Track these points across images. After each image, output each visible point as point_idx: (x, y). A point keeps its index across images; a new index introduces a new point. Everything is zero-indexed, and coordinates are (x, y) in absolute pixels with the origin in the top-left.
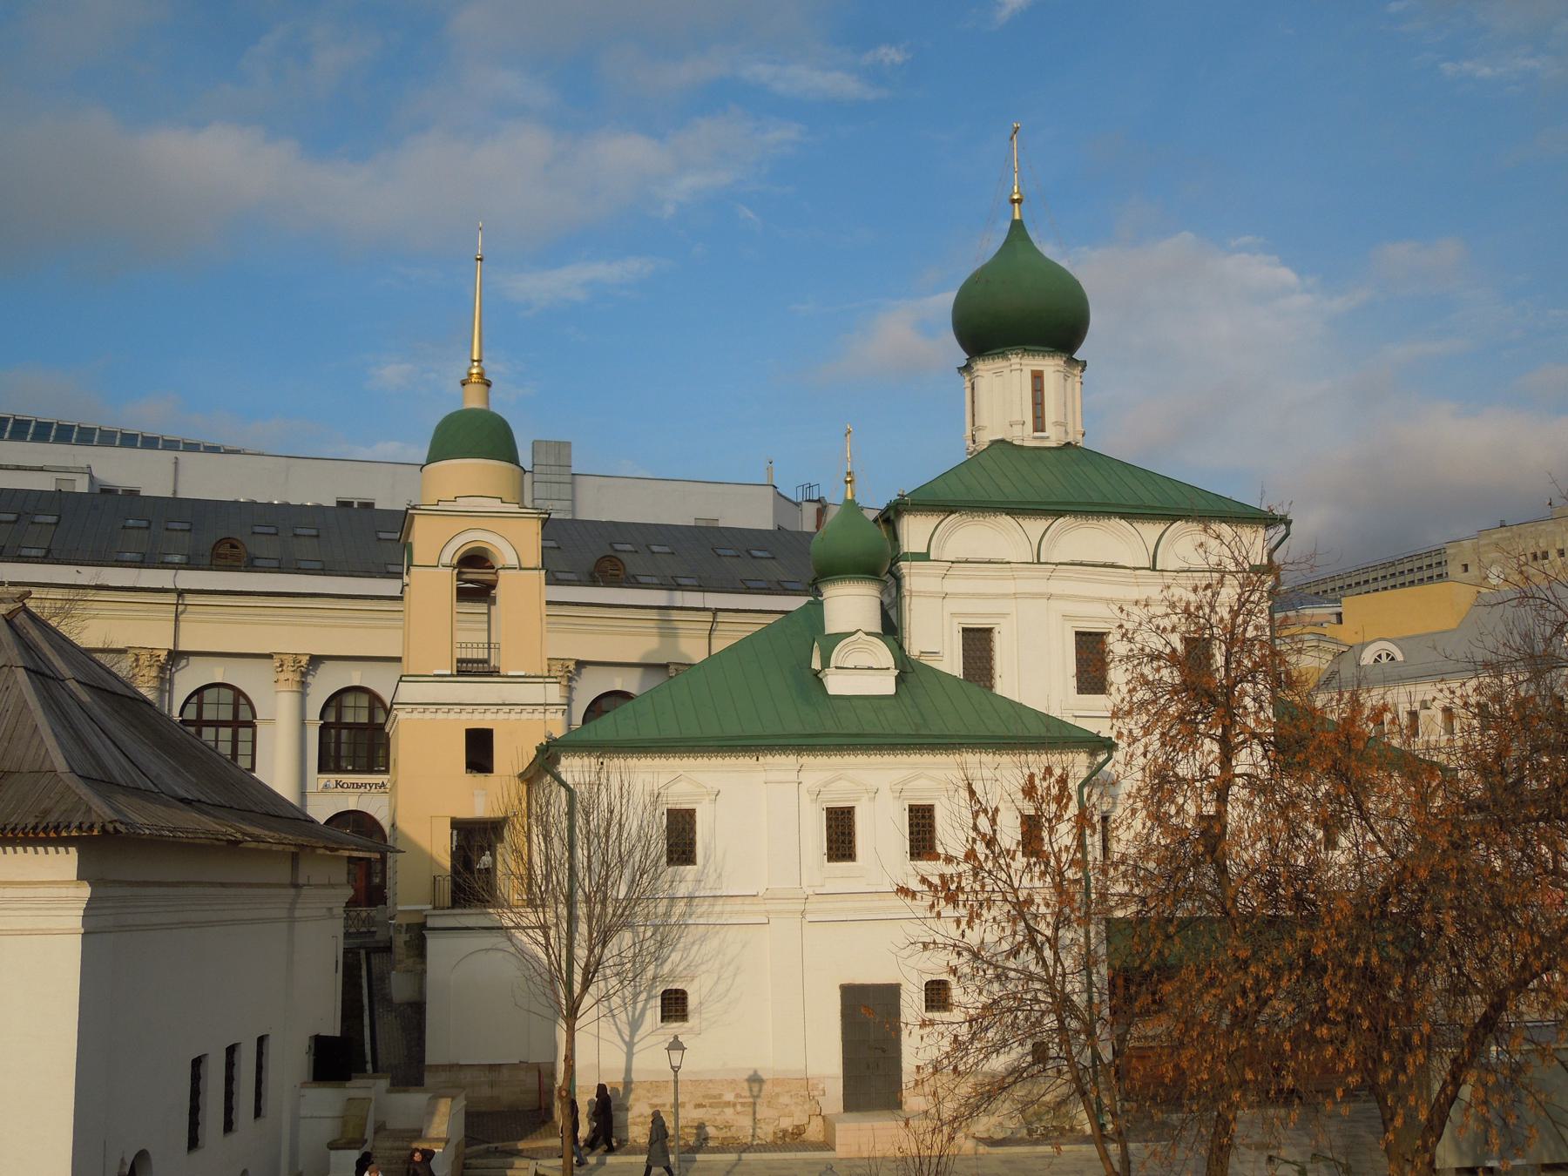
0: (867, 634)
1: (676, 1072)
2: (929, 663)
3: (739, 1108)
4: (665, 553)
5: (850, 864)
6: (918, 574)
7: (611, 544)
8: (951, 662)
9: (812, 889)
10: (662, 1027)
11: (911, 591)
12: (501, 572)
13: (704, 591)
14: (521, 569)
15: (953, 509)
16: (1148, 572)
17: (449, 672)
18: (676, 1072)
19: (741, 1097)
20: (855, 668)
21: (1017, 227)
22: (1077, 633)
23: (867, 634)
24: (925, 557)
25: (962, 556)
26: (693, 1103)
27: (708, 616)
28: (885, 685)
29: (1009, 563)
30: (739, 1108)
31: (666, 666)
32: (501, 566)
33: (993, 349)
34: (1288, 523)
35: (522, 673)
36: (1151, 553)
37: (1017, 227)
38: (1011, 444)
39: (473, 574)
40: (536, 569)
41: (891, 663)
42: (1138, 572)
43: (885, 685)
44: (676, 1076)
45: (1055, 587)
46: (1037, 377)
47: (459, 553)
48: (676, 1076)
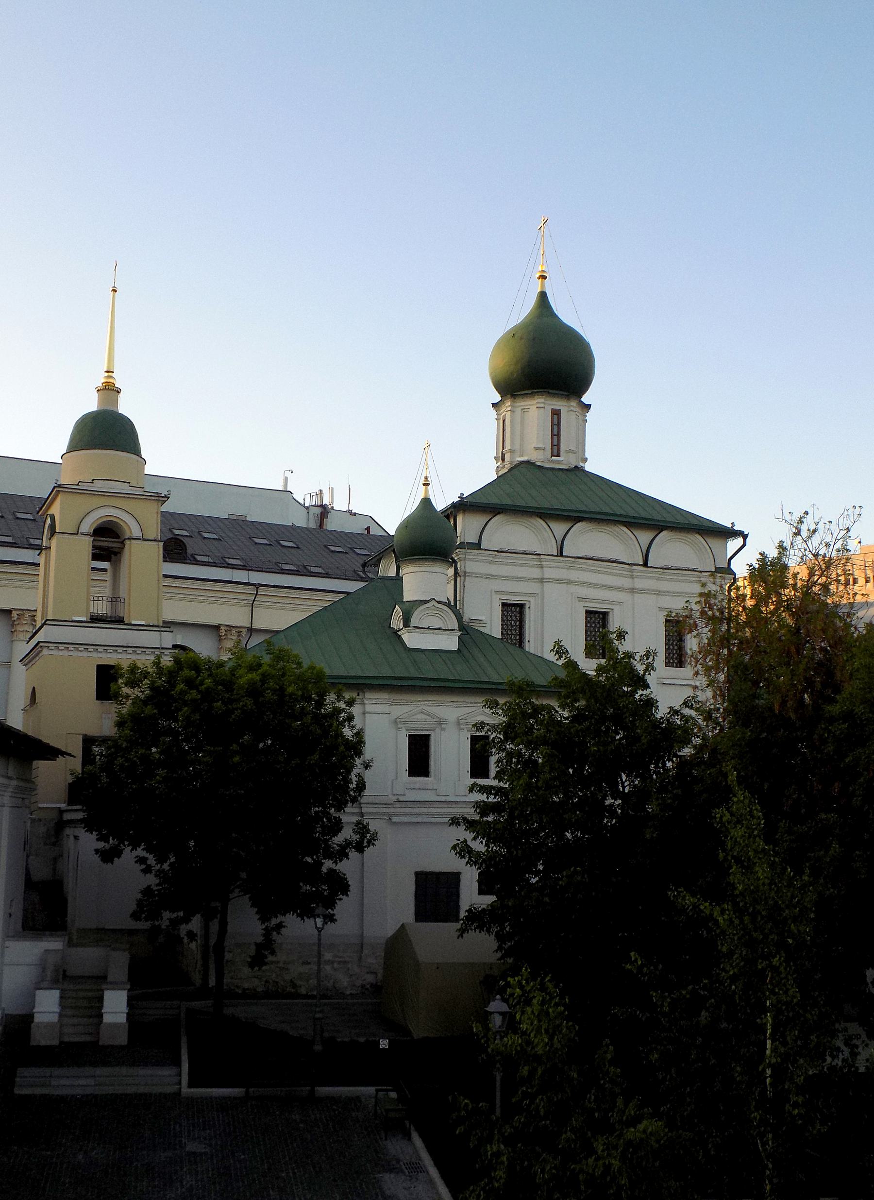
0: (439, 602)
1: (320, 932)
2: (479, 628)
3: (336, 965)
4: (214, 539)
5: (419, 870)
6: (470, 560)
7: (170, 530)
8: (495, 629)
9: (396, 797)
10: (612, 602)
11: (465, 572)
12: (127, 542)
13: (248, 570)
14: (145, 540)
15: (501, 511)
16: (642, 568)
17: (84, 619)
18: (320, 932)
19: (337, 957)
20: (428, 628)
21: (543, 296)
22: (587, 612)
23: (439, 602)
24: (477, 546)
25: (505, 547)
26: (301, 961)
27: (252, 590)
28: (451, 643)
29: (539, 555)
30: (336, 965)
31: (217, 628)
32: (127, 537)
33: (552, 389)
34: (745, 537)
35: (143, 623)
36: (644, 551)
37: (543, 296)
38: (533, 464)
39: (106, 542)
40: (155, 540)
41: (456, 627)
42: (635, 567)
43: (451, 643)
44: (319, 935)
45: (574, 575)
46: (556, 413)
47: (111, 519)
48: (319, 935)
